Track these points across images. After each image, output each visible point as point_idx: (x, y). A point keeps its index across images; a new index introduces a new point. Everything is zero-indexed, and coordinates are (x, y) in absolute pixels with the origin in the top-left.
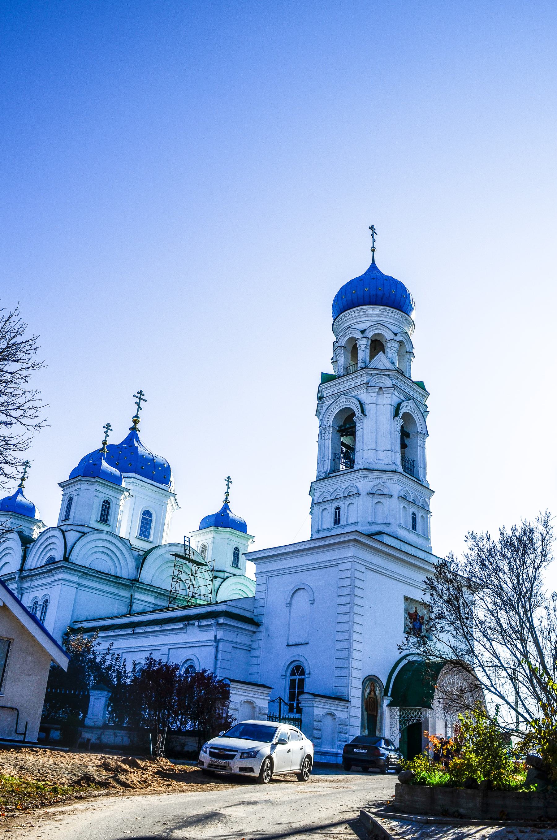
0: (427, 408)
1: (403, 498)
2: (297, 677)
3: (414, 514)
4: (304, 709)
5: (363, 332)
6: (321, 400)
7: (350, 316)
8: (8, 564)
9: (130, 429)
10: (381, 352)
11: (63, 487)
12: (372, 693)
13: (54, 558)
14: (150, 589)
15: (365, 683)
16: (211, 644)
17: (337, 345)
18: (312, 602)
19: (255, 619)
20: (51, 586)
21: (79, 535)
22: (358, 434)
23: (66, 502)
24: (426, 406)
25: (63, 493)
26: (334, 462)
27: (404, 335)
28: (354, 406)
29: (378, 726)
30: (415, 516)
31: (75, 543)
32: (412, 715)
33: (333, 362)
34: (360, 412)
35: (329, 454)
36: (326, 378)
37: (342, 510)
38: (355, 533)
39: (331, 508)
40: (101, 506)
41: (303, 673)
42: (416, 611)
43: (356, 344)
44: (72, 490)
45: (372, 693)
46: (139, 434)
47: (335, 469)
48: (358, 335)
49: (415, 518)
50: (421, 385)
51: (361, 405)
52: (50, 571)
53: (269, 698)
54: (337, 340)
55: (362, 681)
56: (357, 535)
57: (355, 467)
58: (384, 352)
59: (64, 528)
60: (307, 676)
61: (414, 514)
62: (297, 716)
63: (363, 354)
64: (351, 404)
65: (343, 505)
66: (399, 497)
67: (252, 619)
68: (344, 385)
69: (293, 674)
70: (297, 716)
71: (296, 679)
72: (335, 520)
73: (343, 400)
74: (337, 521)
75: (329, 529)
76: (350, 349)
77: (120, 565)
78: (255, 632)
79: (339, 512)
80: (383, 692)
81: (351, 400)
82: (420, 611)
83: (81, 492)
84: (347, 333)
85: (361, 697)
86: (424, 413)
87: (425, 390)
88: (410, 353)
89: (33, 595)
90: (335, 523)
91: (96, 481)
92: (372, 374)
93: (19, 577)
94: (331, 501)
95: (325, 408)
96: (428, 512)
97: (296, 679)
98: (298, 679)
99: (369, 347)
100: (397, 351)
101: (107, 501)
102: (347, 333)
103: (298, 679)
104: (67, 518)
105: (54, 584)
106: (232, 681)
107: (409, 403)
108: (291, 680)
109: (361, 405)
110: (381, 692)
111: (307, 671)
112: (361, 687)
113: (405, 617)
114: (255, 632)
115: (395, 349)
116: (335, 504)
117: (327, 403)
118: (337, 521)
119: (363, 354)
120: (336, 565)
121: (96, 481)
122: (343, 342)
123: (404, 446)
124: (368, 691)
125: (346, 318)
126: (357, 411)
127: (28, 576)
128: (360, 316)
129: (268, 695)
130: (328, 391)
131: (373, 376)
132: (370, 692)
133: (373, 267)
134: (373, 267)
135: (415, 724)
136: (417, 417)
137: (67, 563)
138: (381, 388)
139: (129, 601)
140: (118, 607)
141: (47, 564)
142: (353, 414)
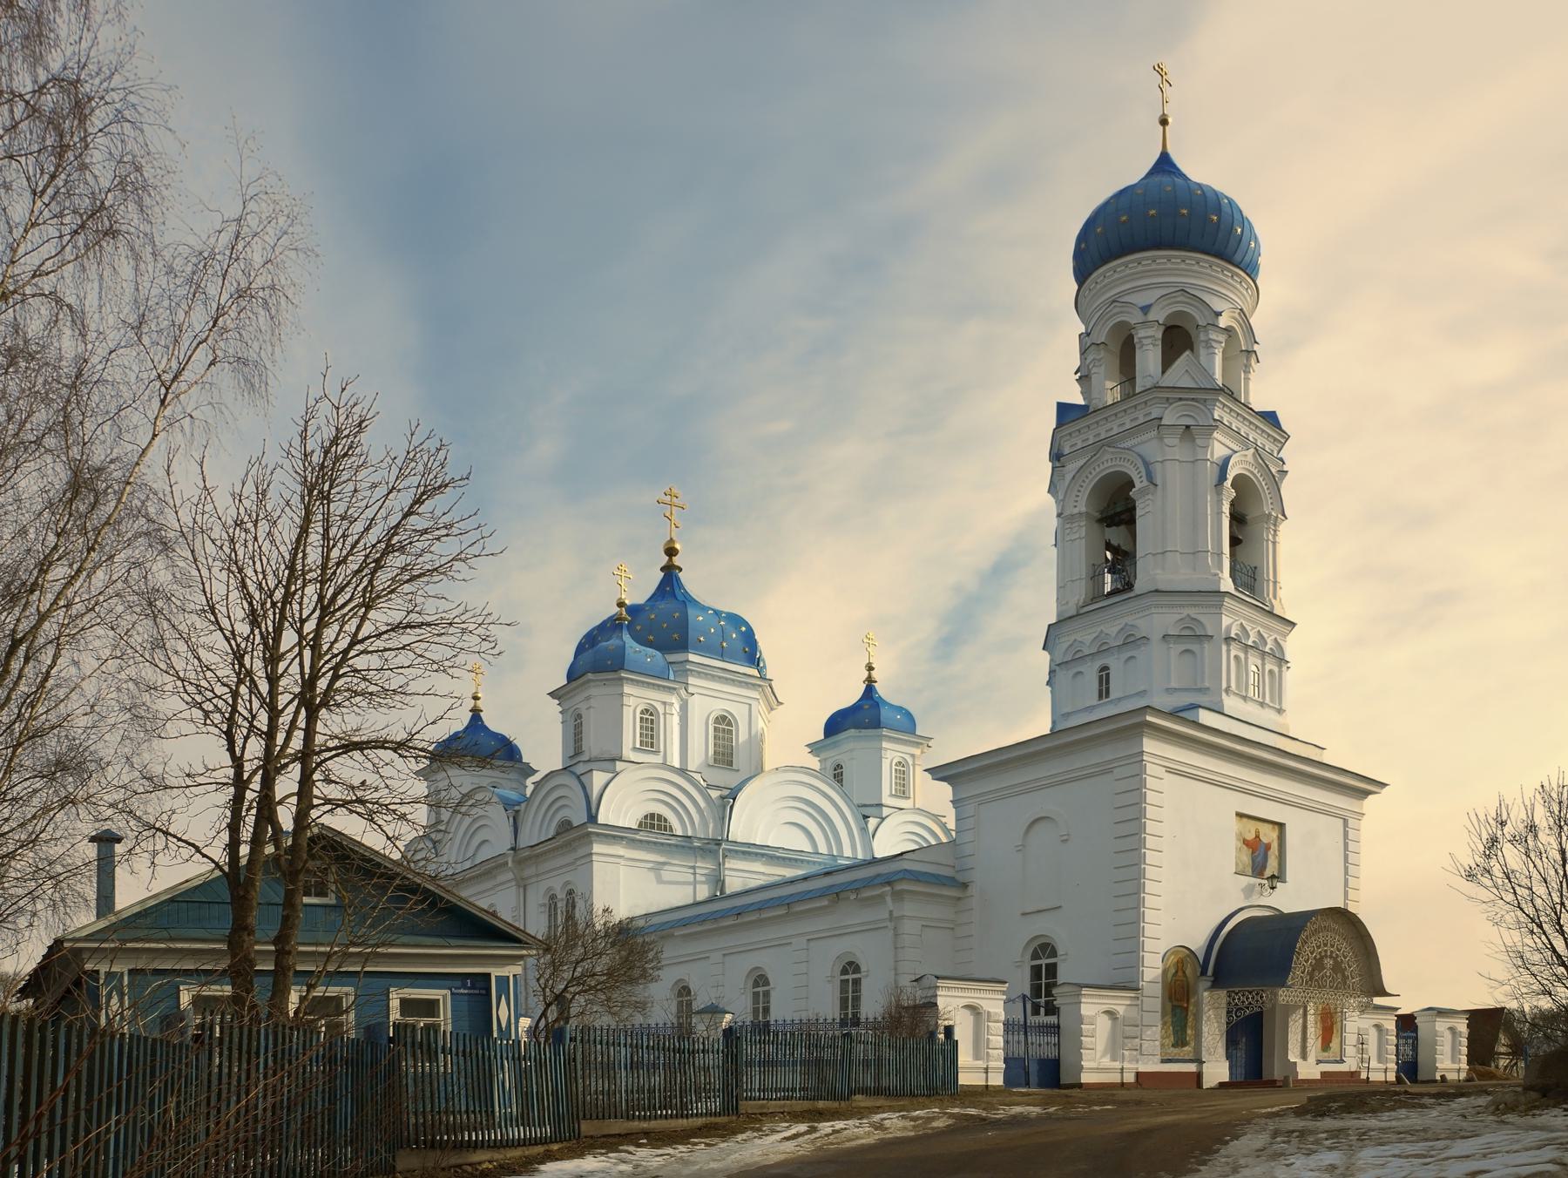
2: (850, 977)
4: (1063, 1009)
5: (1146, 309)
6: (1059, 461)
7: (1116, 276)
8: (487, 844)
9: (662, 569)
11: (559, 699)
12: (1180, 973)
13: (569, 823)
14: (751, 852)
16: (885, 924)
17: (1089, 341)
18: (1065, 838)
19: (960, 878)
20: (573, 867)
23: (572, 723)
24: (1281, 460)
25: (561, 709)
31: (602, 795)
33: (1080, 377)
34: (1144, 478)
35: (1081, 570)
39: (1091, 672)
40: (638, 720)
42: (1257, 836)
43: (1131, 337)
45: (1180, 973)
46: (680, 575)
47: (1097, 595)
48: (1134, 318)
50: (1271, 418)
51: (1147, 464)
52: (568, 844)
53: (1005, 997)
54: (1086, 329)
55: (1161, 956)
57: (1136, 586)
58: (1192, 350)
59: (580, 769)
60: (1063, 957)
62: (1052, 1019)
63: (1149, 358)
64: (1125, 464)
65: (1115, 663)
67: (953, 879)
68: (1109, 426)
69: (1035, 956)
70: (1052, 1019)
73: (1108, 456)
74: (1104, 691)
75: (1091, 708)
76: (1116, 347)
79: (1108, 675)
81: (1123, 456)
83: (592, 702)
87: (1280, 429)
88: (1250, 353)
89: (544, 886)
90: (1100, 697)
92: (1168, 399)
93: (513, 861)
95: (1068, 477)
96: (1281, 661)
98: (1046, 965)
99: (1160, 343)
103: (1046, 965)
104: (578, 751)
105: (578, 863)
106: (938, 978)
108: (842, 981)
109: (1147, 464)
111: (1060, 952)
114: (959, 899)
116: (1098, 664)
118: (1104, 691)
119: (1149, 358)
120: (1110, 771)
125: (1106, 281)
126: (1140, 483)
127: (529, 858)
129: (1003, 993)
131: (1171, 404)
132: (1177, 972)
133: (1164, 164)
134: (1164, 164)
138: (1188, 427)
141: (558, 834)
142: (1131, 484)
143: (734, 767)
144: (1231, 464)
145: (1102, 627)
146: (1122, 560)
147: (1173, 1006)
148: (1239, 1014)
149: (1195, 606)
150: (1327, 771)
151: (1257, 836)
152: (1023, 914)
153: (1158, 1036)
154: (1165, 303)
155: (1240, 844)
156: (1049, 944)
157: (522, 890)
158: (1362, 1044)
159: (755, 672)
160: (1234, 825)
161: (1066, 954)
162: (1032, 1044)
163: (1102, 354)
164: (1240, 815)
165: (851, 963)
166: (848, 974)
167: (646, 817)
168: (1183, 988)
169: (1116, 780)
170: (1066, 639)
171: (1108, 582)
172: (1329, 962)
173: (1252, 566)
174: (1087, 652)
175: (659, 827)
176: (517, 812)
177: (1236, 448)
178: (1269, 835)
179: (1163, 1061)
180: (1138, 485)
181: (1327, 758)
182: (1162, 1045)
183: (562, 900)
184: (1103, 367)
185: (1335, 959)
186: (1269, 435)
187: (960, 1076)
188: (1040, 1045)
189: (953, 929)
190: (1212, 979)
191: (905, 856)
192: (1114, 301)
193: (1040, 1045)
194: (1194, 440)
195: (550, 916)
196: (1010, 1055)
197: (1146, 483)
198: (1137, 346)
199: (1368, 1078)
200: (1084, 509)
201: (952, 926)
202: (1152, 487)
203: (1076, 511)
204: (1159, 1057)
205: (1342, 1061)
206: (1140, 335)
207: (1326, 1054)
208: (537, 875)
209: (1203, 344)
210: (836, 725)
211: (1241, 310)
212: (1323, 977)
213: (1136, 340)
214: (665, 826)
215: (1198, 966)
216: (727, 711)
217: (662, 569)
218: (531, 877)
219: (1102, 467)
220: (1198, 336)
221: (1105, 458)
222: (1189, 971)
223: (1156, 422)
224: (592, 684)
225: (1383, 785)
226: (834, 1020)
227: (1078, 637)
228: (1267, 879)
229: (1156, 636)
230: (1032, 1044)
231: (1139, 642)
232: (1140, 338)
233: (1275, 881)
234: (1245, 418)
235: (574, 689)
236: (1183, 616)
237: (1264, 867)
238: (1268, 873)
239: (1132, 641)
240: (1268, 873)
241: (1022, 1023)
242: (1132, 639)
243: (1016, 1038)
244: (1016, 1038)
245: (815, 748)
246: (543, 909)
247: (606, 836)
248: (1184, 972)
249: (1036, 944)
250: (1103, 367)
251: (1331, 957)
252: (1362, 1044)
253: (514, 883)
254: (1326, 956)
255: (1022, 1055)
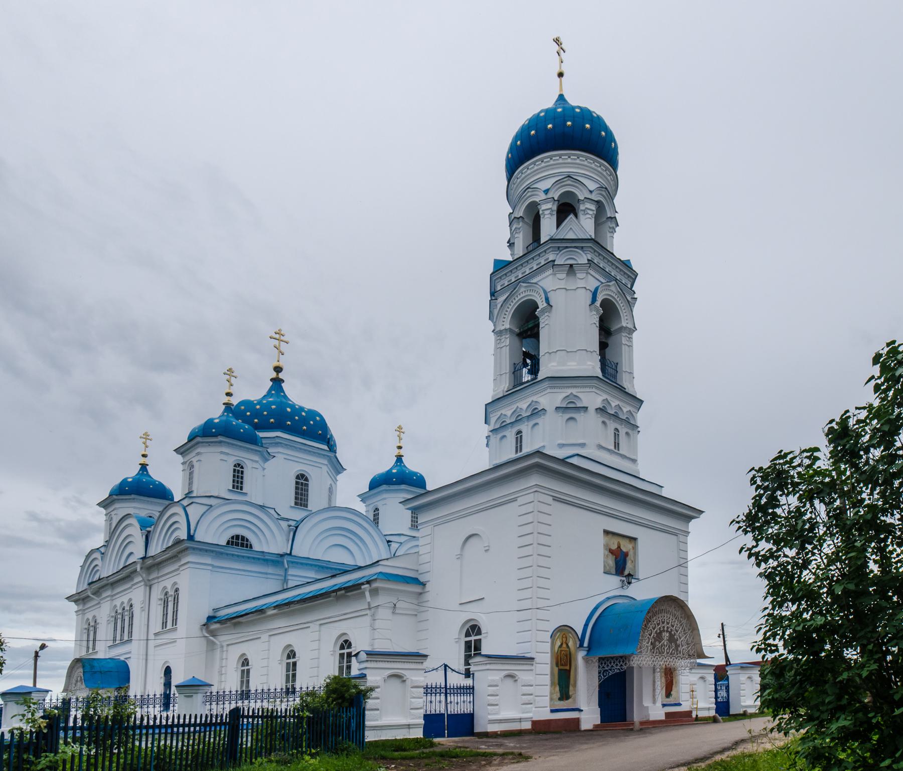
0: (635, 293)
1: (601, 410)
2: (473, 638)
3: (616, 430)
6: (494, 296)
9: (271, 380)
10: (572, 216)
12: (564, 645)
15: (555, 636)
18: (487, 548)
20: (178, 572)
21: (207, 508)
22: (543, 334)
26: (513, 375)
27: (604, 193)
28: (539, 299)
29: (572, 681)
30: (618, 432)
32: (612, 664)
35: (507, 368)
36: (500, 267)
37: (524, 434)
38: (538, 454)
39: (510, 434)
41: (479, 632)
42: (619, 547)
44: (191, 456)
45: (564, 645)
46: (283, 385)
49: (618, 435)
50: (626, 264)
55: (550, 634)
56: (540, 458)
60: (485, 635)
61: (616, 430)
65: (525, 428)
66: (596, 409)
69: (468, 634)
70: (468, 682)
71: (471, 641)
72: (517, 447)
73: (522, 290)
77: (266, 538)
78: (421, 594)
79: (521, 437)
80: (578, 643)
82: (624, 546)
84: (526, 197)
85: (549, 651)
86: (631, 304)
89: (162, 585)
91: (220, 442)
92: (559, 248)
94: (510, 425)
95: (499, 306)
97: (471, 641)
99: (555, 213)
100: (594, 216)
101: (239, 465)
102: (526, 197)
105: (181, 569)
107: (609, 286)
110: (575, 643)
112: (549, 640)
113: (604, 555)
114: (421, 594)
115: (591, 212)
116: (515, 430)
117: (501, 299)
120: (515, 500)
121: (220, 442)
122: (520, 213)
123: (603, 346)
124: (558, 643)
125: (523, 176)
126: (542, 305)
128: (543, 170)
130: (502, 281)
131: (560, 251)
132: (562, 644)
133: (561, 97)
134: (561, 97)
135: (617, 674)
136: (621, 305)
137: (194, 543)
138: (571, 266)
139: (283, 578)
140: (272, 585)
143: (244, 491)
144: (598, 293)
145: (518, 404)
146: (531, 360)
147: (560, 670)
148: (605, 674)
149: (576, 387)
150: (656, 499)
151: (619, 547)
152: (460, 604)
153: (548, 693)
154: (557, 187)
155: (607, 552)
156: (476, 625)
157: (148, 588)
158: (693, 691)
159: (326, 447)
160: (601, 539)
161: (487, 633)
162: (451, 702)
163: (521, 224)
164: (607, 532)
165: (346, 641)
166: (290, 658)
167: (233, 537)
168: (566, 656)
169: (519, 506)
170: (494, 414)
171: (526, 377)
172: (666, 635)
173: (615, 362)
174: (508, 422)
175: (242, 545)
176: (149, 532)
177: (603, 281)
178: (626, 546)
179: (552, 711)
180: (541, 307)
181: (665, 493)
182: (551, 699)
183: (171, 596)
184: (521, 233)
185: (670, 633)
186: (625, 273)
187: (367, 733)
188: (457, 703)
189: (416, 615)
190: (587, 649)
191: (380, 563)
192: (528, 188)
193: (457, 703)
194: (575, 274)
195: (164, 607)
196: (428, 713)
197: (545, 305)
198: (542, 216)
199: (697, 716)
200: (507, 326)
201: (415, 613)
202: (549, 307)
203: (503, 328)
204: (548, 709)
205: (680, 704)
206: (543, 208)
207: (668, 699)
208: (158, 578)
209: (583, 212)
210: (376, 484)
211: (606, 188)
212: (662, 646)
213: (541, 212)
214: (247, 545)
215: (577, 640)
216: (301, 470)
217: (271, 380)
218: (153, 579)
219: (519, 297)
220: (579, 208)
221: (521, 291)
222: (571, 644)
223: (551, 264)
224: (200, 444)
225: (702, 512)
226: (282, 689)
227: (503, 412)
228: (626, 576)
229: (550, 409)
230: (451, 702)
231: (540, 413)
232: (543, 210)
233: (630, 578)
234: (609, 261)
235: (371, 496)
236: (568, 394)
237: (624, 568)
238: (626, 573)
239: (536, 412)
240: (626, 573)
241: (443, 686)
242: (536, 411)
243: (438, 697)
244: (438, 697)
245: (364, 498)
246: (160, 602)
247: (201, 550)
248: (567, 645)
249: (468, 626)
250: (521, 233)
251: (667, 631)
252: (693, 691)
253: (142, 583)
254: (664, 631)
255: (443, 711)
